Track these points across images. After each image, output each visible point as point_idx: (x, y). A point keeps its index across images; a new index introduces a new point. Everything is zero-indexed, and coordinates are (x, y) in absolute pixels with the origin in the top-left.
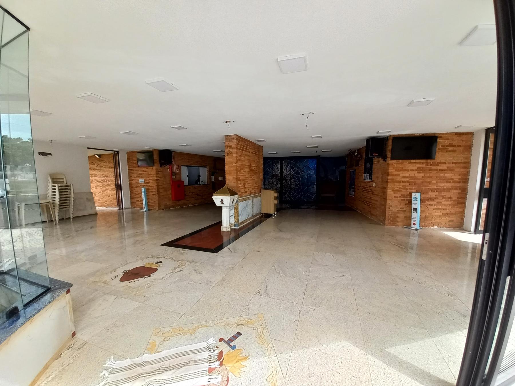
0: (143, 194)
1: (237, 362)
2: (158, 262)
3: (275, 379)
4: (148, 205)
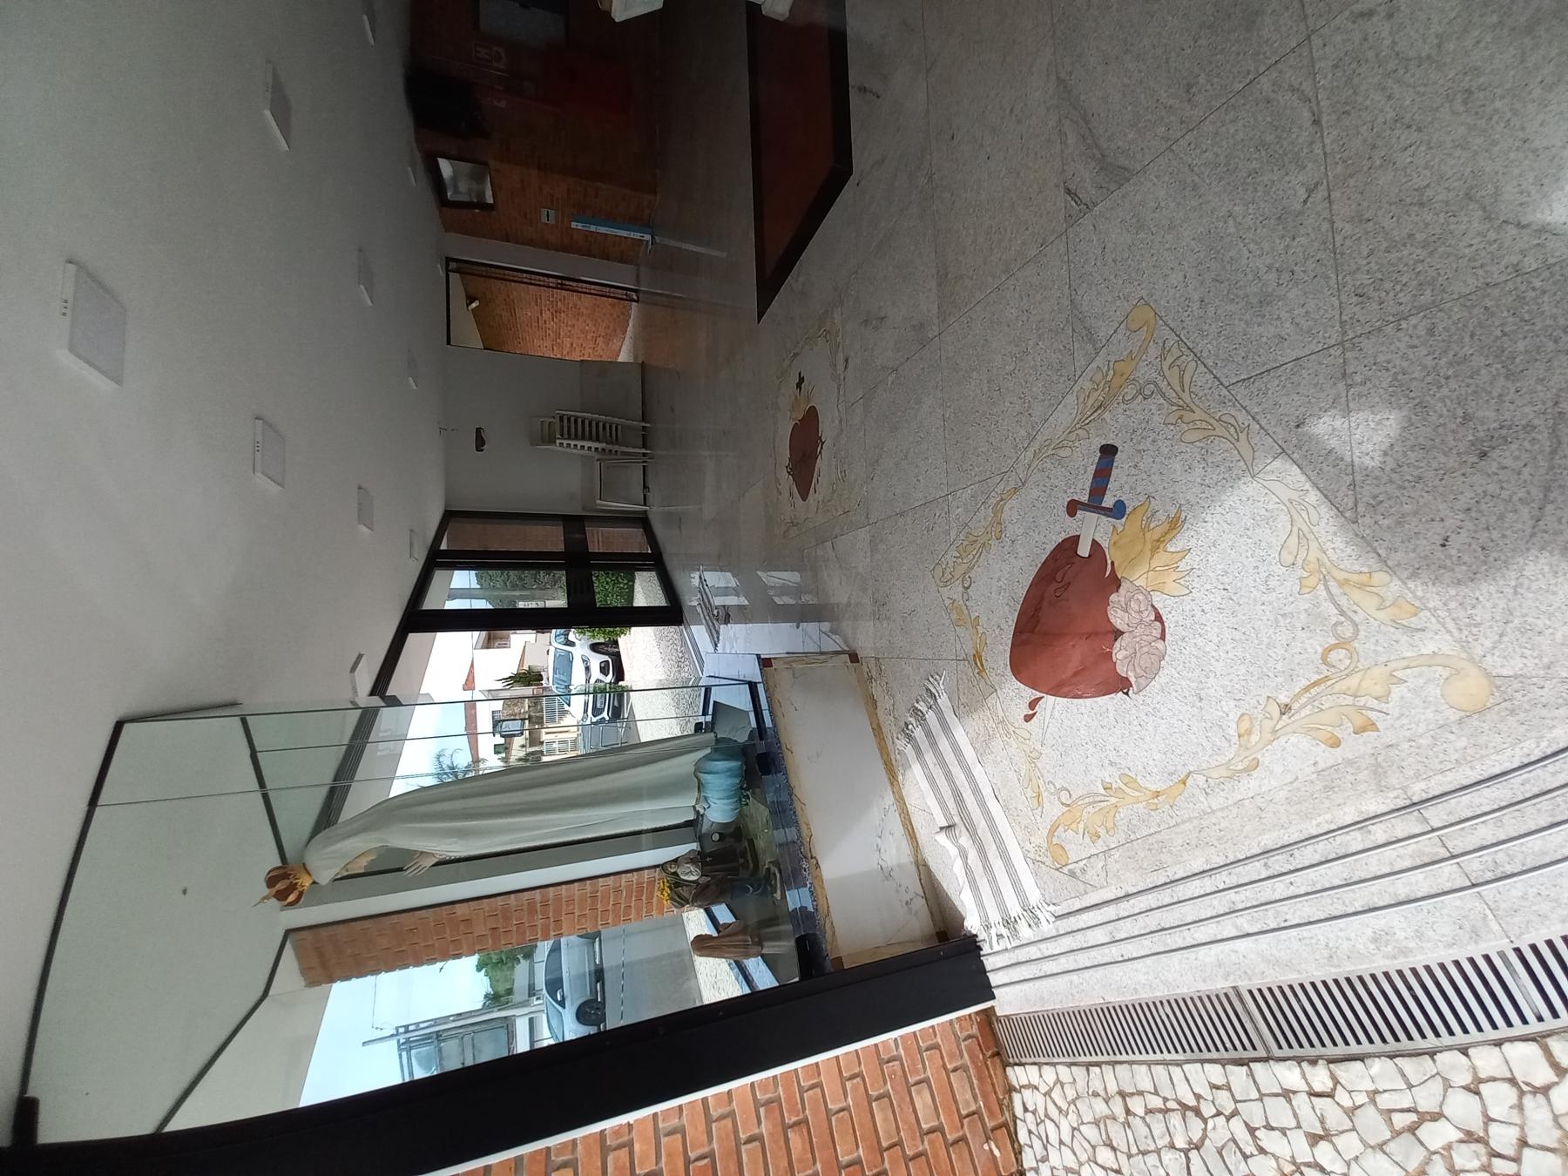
0: (593, 228)
1: (1154, 550)
2: (799, 386)
3: (1314, 545)
4: (633, 221)
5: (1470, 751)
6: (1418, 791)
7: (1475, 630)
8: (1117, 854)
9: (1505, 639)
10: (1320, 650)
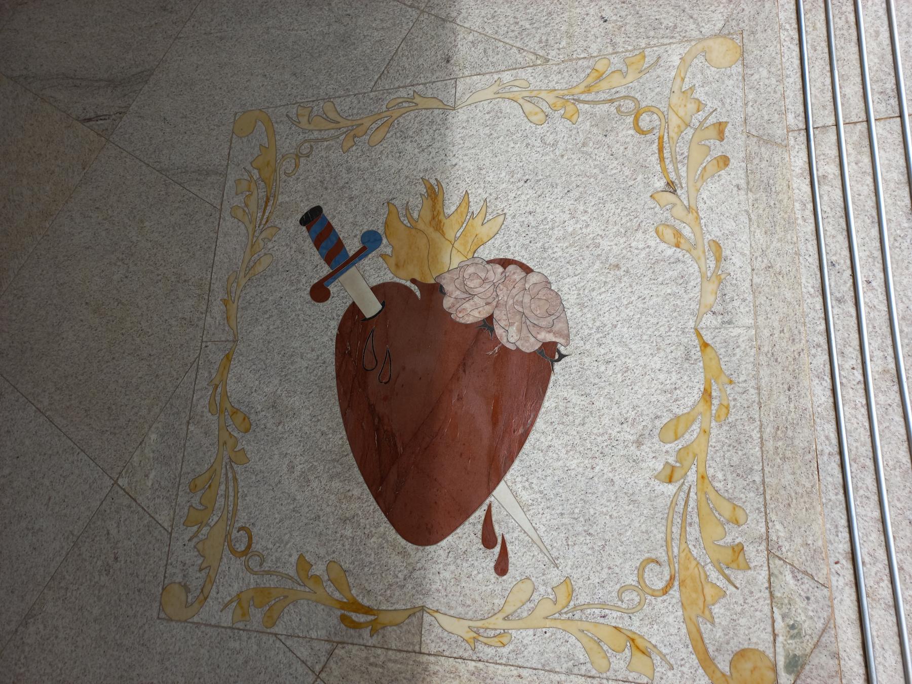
3: (543, 95)
5: (773, 70)
6: (794, 120)
7: (678, 30)
8: (779, 531)
9: (695, 16)
10: (632, 132)
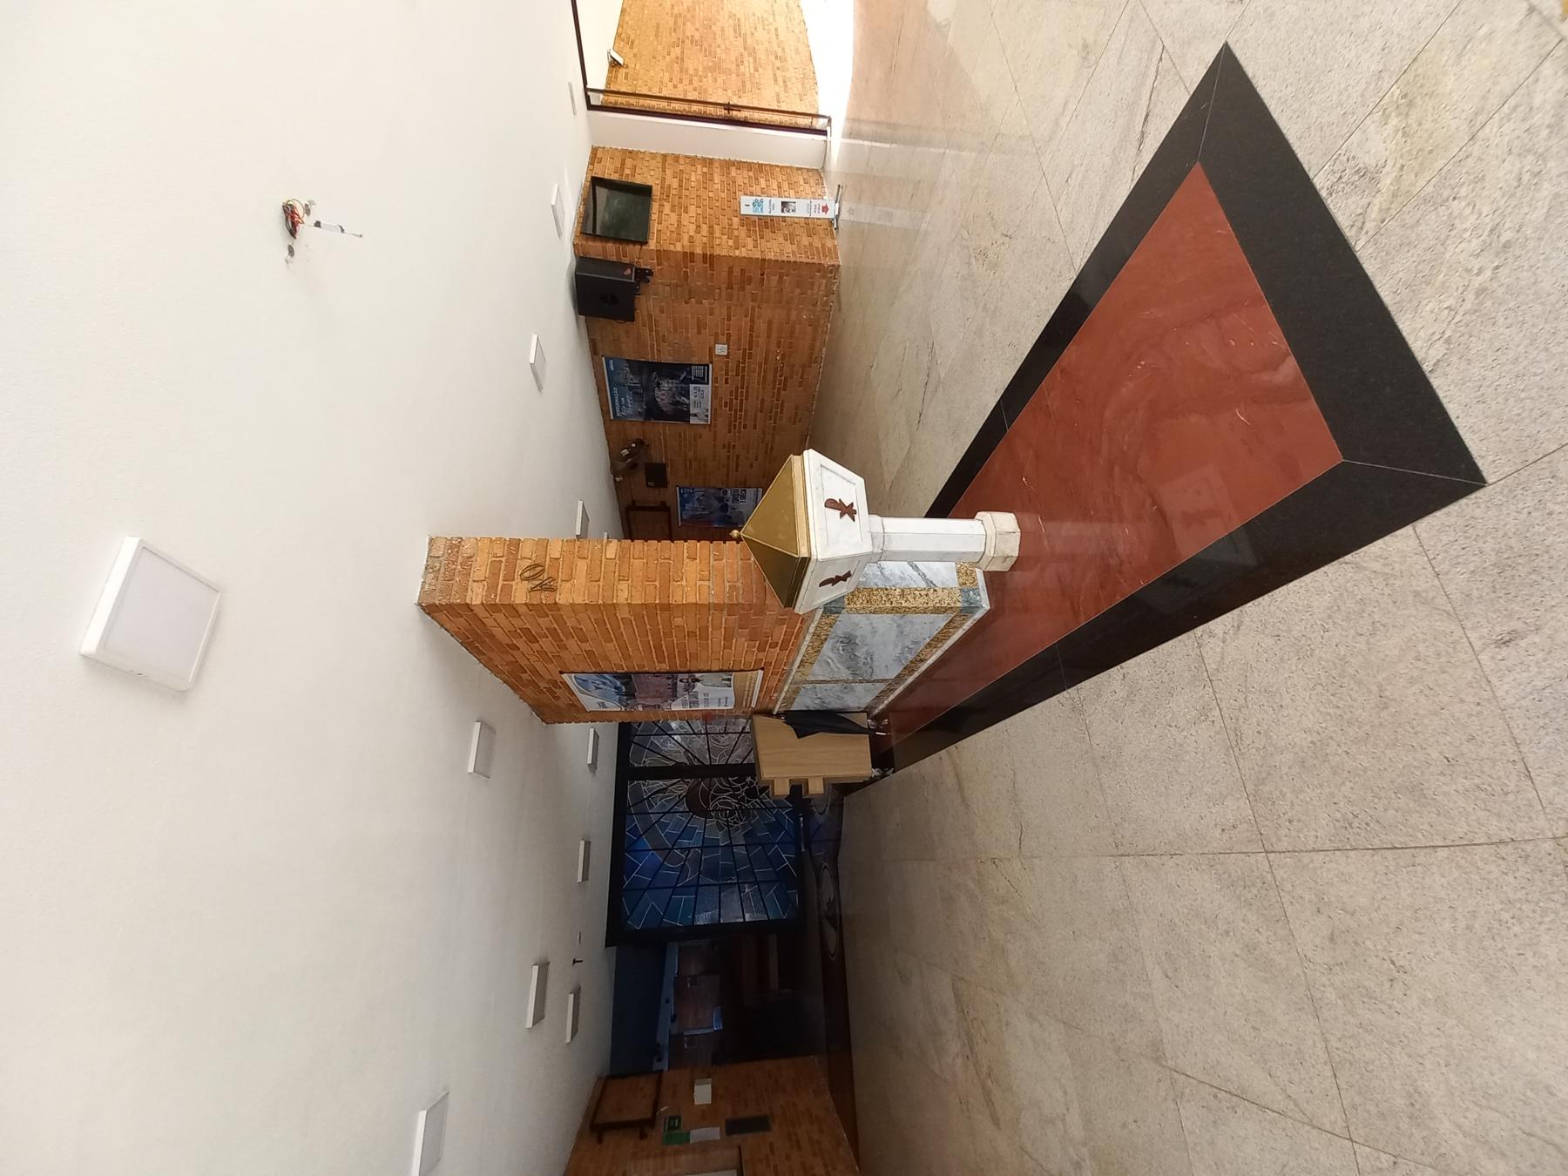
0: (812, 630)
